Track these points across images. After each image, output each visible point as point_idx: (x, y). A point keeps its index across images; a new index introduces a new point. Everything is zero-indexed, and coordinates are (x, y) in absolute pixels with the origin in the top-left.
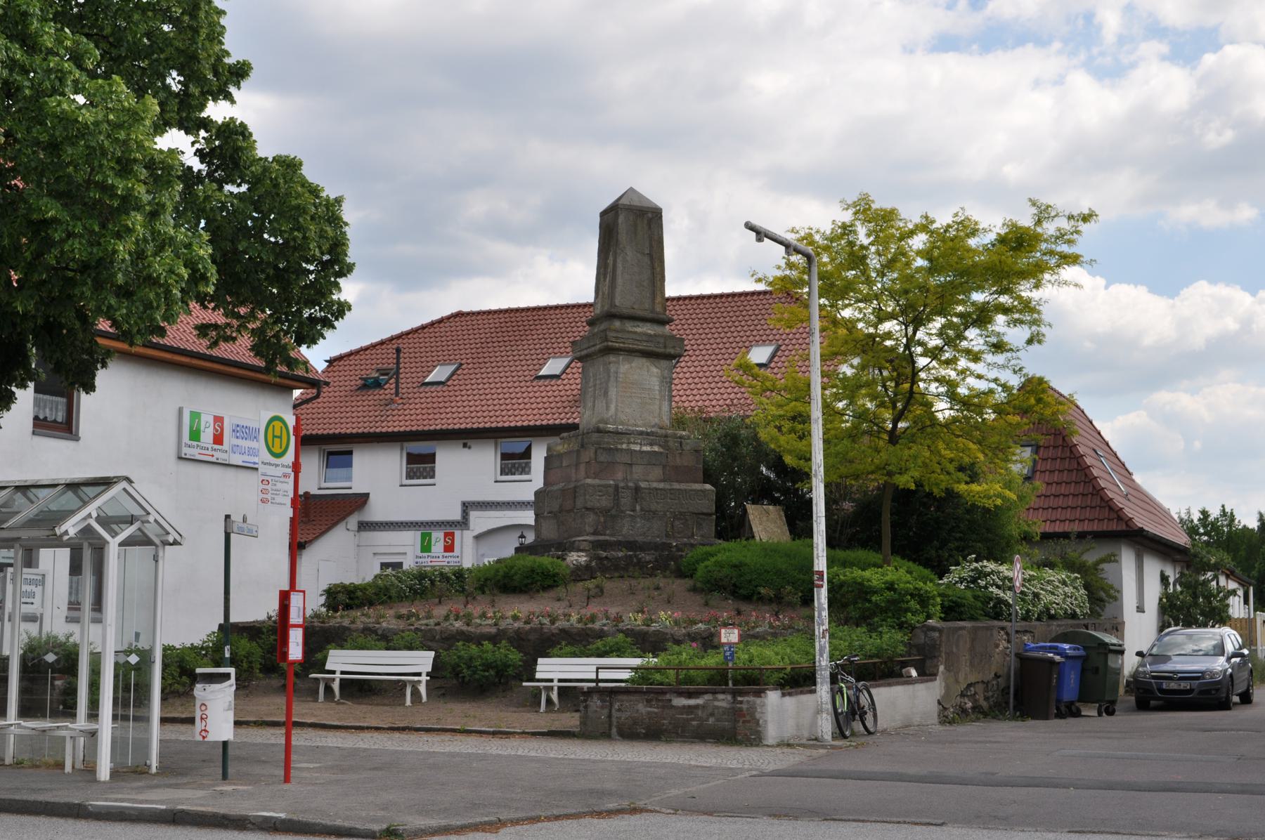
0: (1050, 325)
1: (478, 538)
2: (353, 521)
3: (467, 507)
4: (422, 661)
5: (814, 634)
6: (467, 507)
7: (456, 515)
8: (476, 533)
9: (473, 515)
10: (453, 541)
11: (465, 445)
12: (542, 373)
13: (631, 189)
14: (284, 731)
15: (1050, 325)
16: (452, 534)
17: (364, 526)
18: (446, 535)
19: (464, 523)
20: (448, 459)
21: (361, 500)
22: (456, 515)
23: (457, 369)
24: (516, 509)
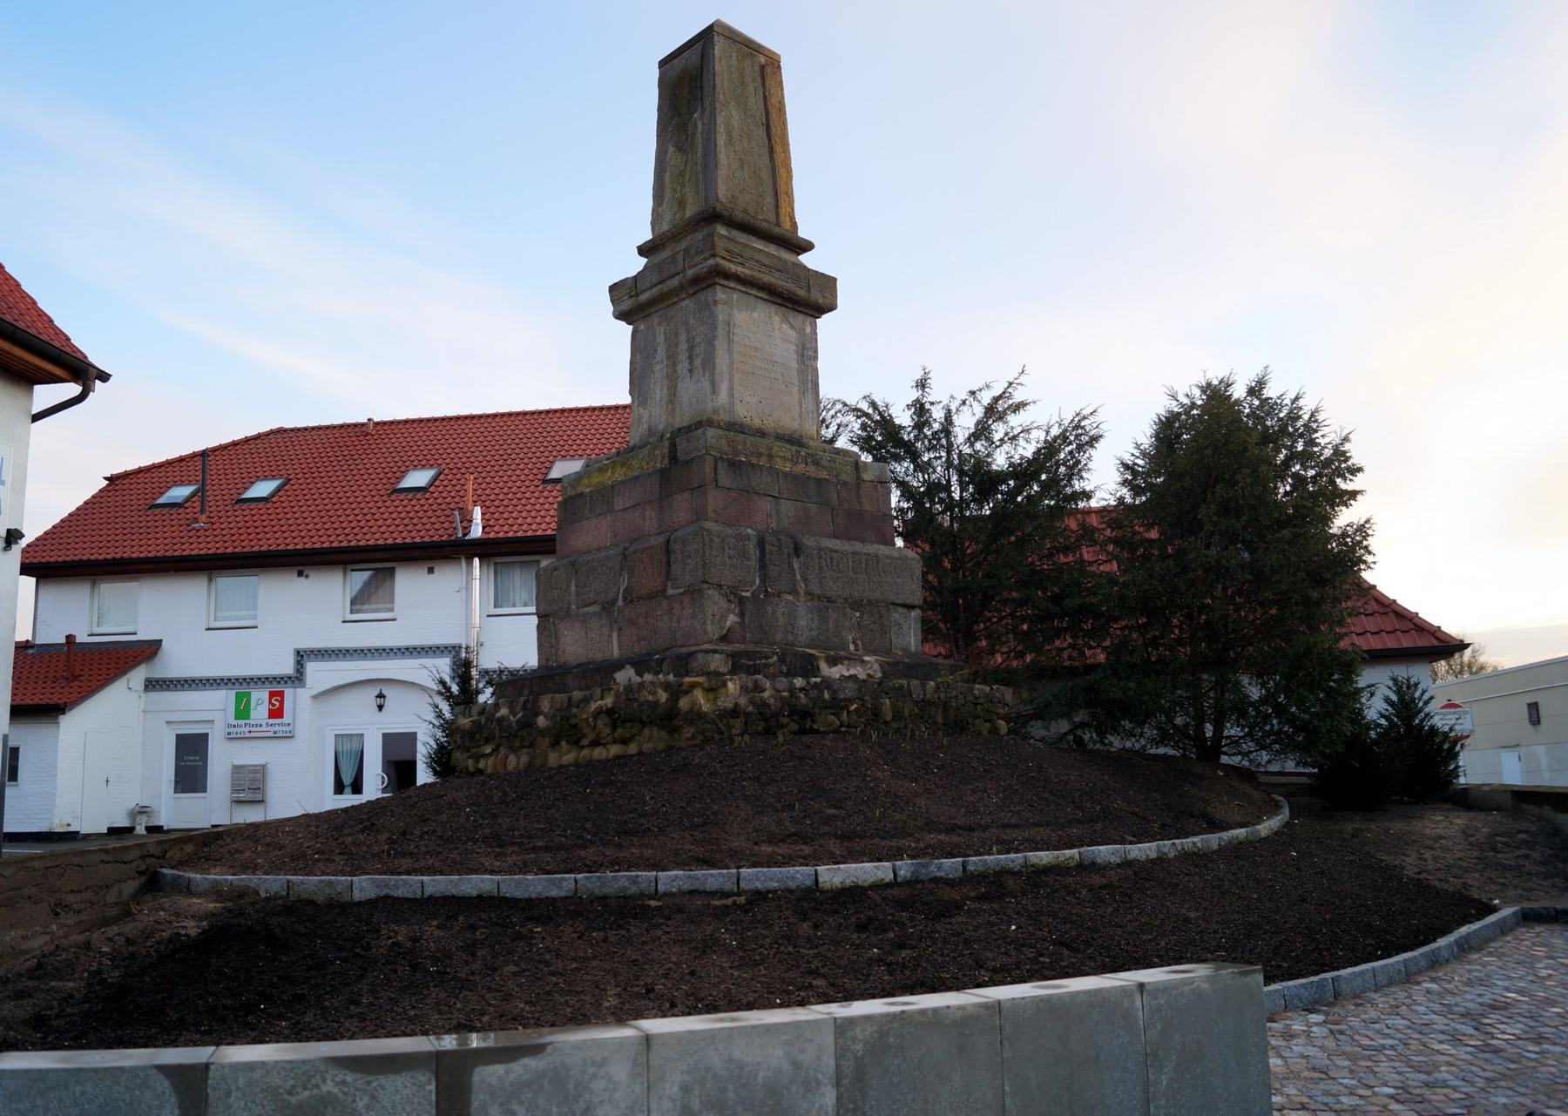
0: (922, 384)
1: (315, 697)
2: (138, 676)
3: (301, 656)
4: (1224, 759)
5: (880, 860)
6: (301, 656)
7: (288, 668)
8: (315, 692)
9: (311, 667)
10: (282, 703)
11: (300, 574)
12: (160, 501)
13: (834, 280)
14: (742, 884)
15: (922, 384)
16: (281, 694)
17: (152, 685)
18: (272, 694)
19: (298, 678)
20: (410, 584)
21: (149, 650)
22: (288, 668)
23: (284, 484)
24: (373, 658)
